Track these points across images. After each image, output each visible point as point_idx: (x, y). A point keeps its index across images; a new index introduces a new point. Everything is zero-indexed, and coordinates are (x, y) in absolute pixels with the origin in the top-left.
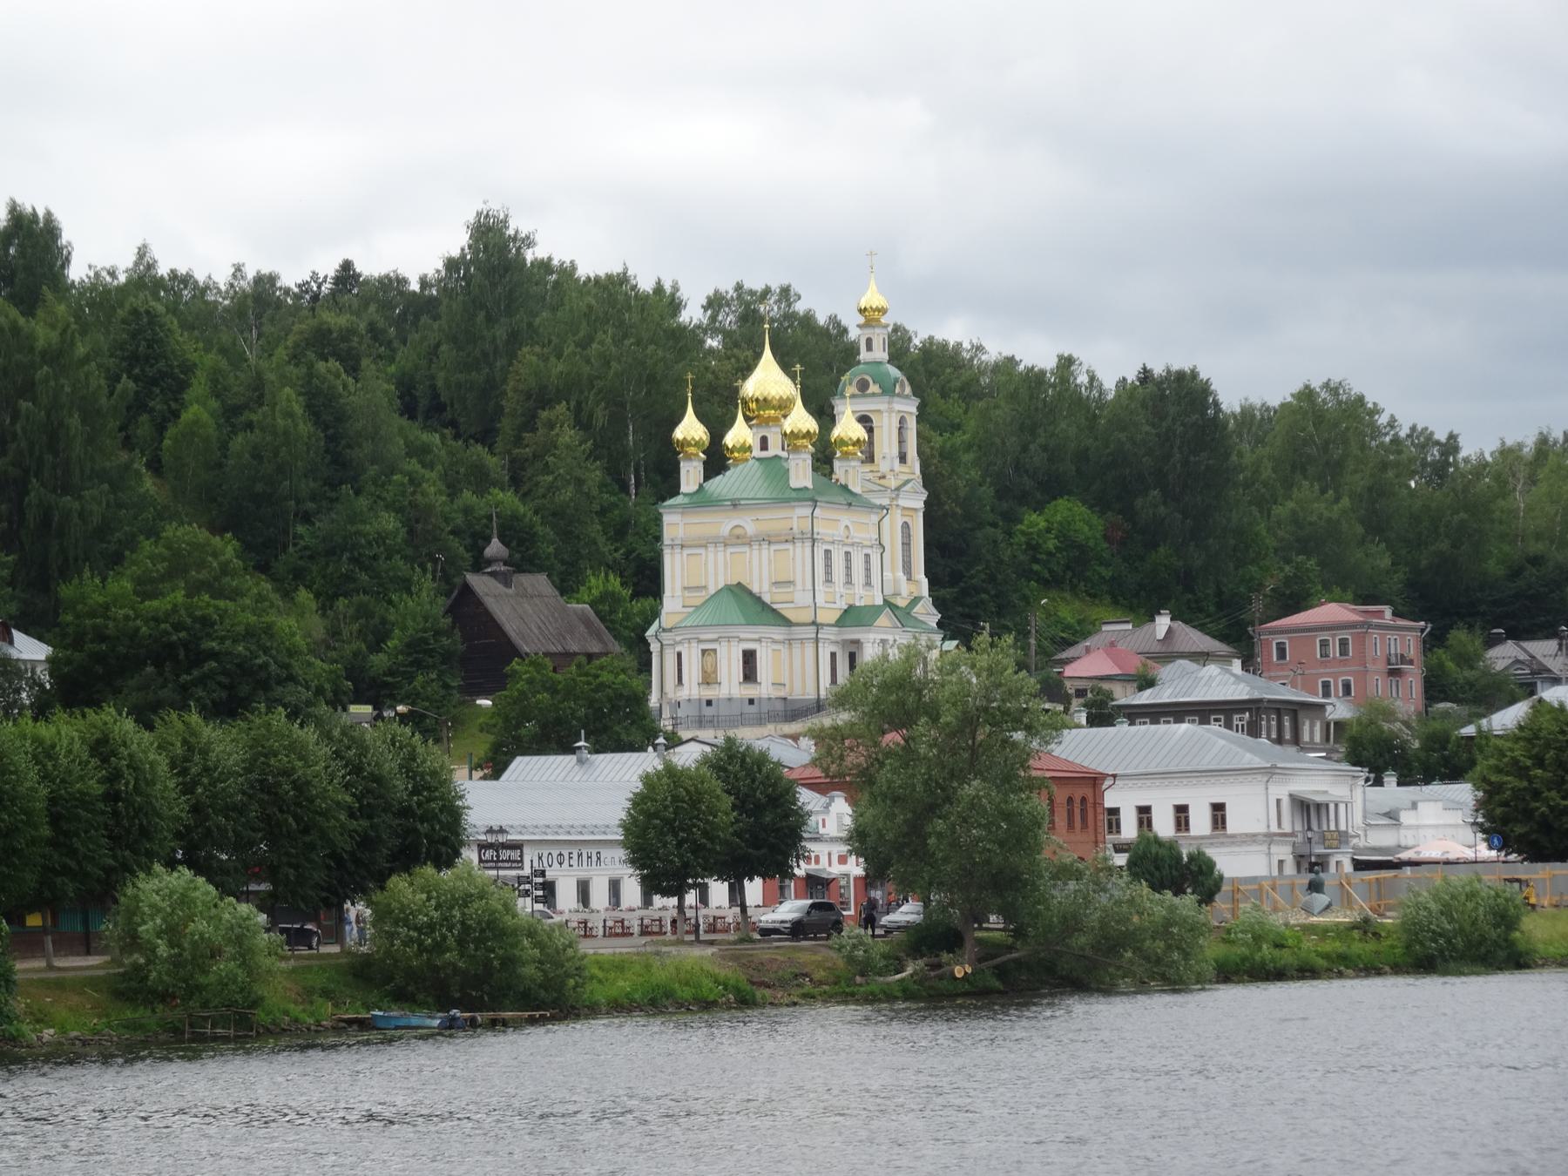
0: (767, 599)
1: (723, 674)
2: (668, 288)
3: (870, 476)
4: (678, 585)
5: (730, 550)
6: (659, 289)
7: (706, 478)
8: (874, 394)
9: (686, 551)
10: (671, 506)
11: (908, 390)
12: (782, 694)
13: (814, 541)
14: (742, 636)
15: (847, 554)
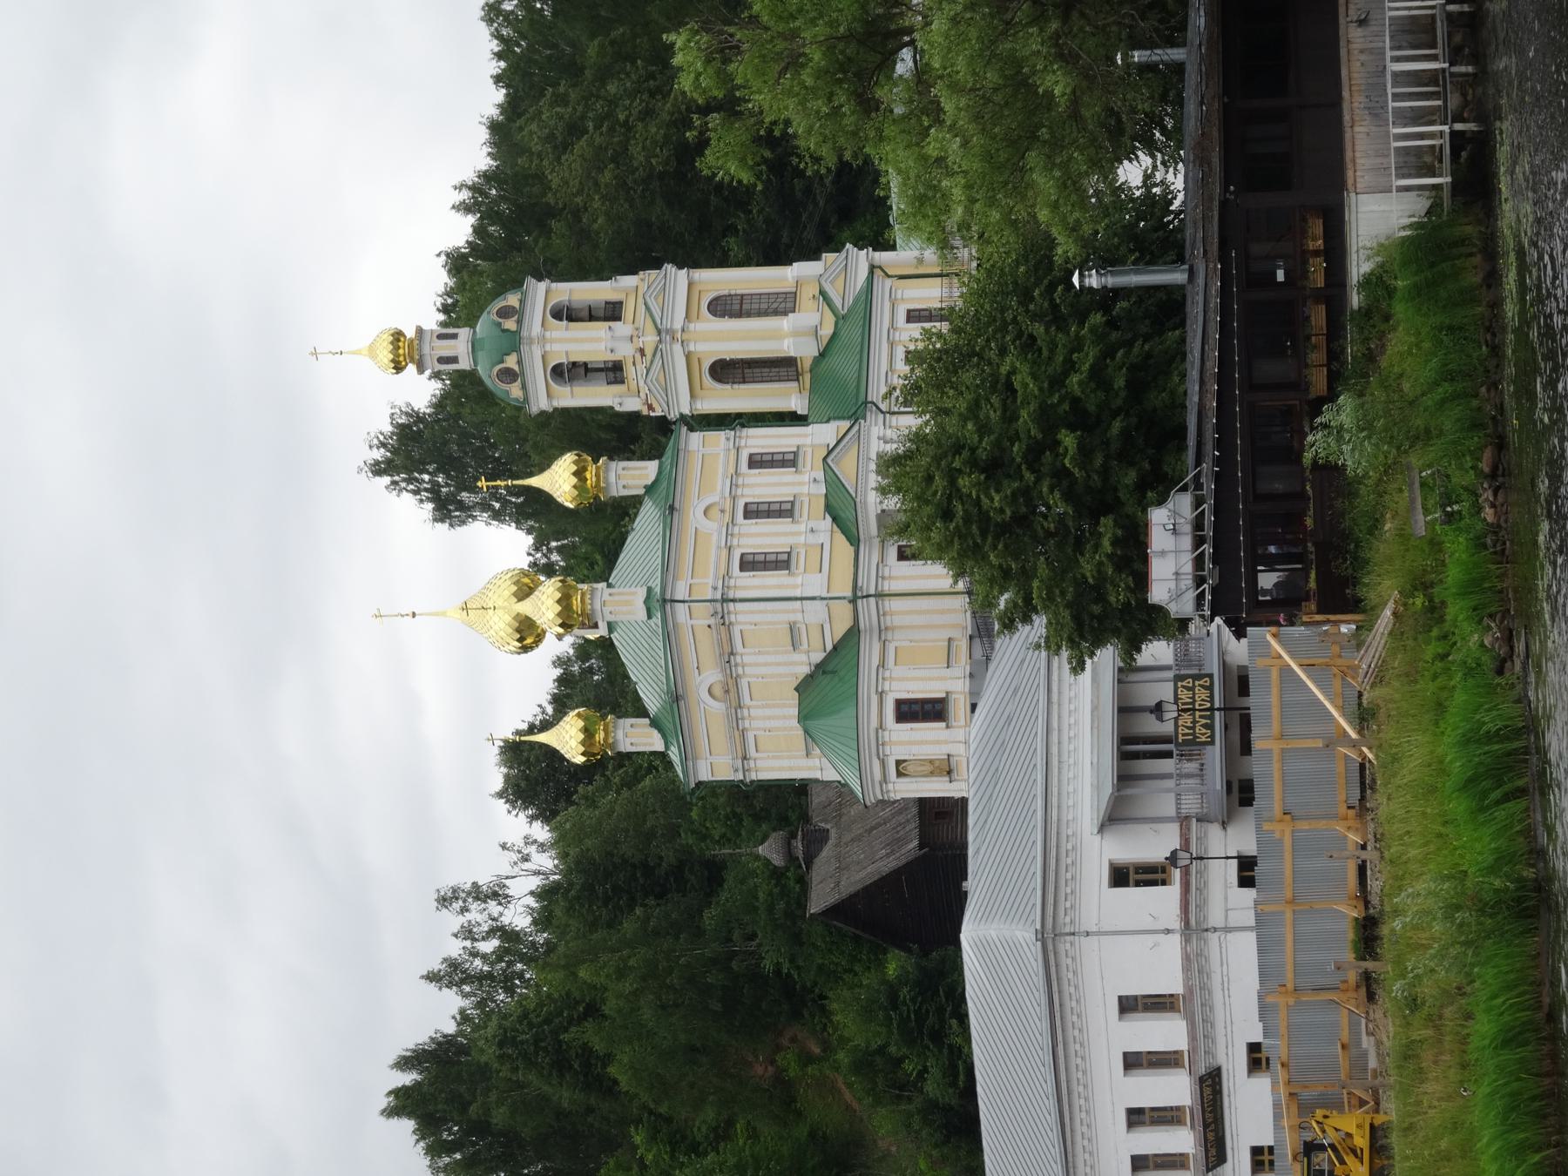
0: (818, 657)
1: (938, 752)
2: (465, 195)
3: (641, 368)
4: (804, 762)
5: (747, 700)
6: (465, 208)
7: (642, 712)
8: (520, 362)
9: (752, 752)
10: (685, 772)
11: (512, 300)
12: (962, 645)
13: (725, 600)
14: (874, 723)
15: (748, 514)
